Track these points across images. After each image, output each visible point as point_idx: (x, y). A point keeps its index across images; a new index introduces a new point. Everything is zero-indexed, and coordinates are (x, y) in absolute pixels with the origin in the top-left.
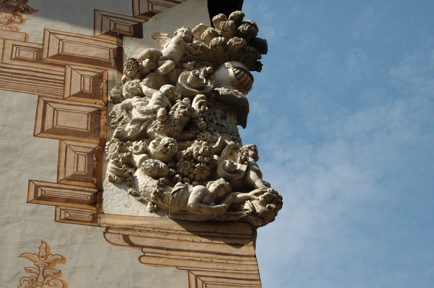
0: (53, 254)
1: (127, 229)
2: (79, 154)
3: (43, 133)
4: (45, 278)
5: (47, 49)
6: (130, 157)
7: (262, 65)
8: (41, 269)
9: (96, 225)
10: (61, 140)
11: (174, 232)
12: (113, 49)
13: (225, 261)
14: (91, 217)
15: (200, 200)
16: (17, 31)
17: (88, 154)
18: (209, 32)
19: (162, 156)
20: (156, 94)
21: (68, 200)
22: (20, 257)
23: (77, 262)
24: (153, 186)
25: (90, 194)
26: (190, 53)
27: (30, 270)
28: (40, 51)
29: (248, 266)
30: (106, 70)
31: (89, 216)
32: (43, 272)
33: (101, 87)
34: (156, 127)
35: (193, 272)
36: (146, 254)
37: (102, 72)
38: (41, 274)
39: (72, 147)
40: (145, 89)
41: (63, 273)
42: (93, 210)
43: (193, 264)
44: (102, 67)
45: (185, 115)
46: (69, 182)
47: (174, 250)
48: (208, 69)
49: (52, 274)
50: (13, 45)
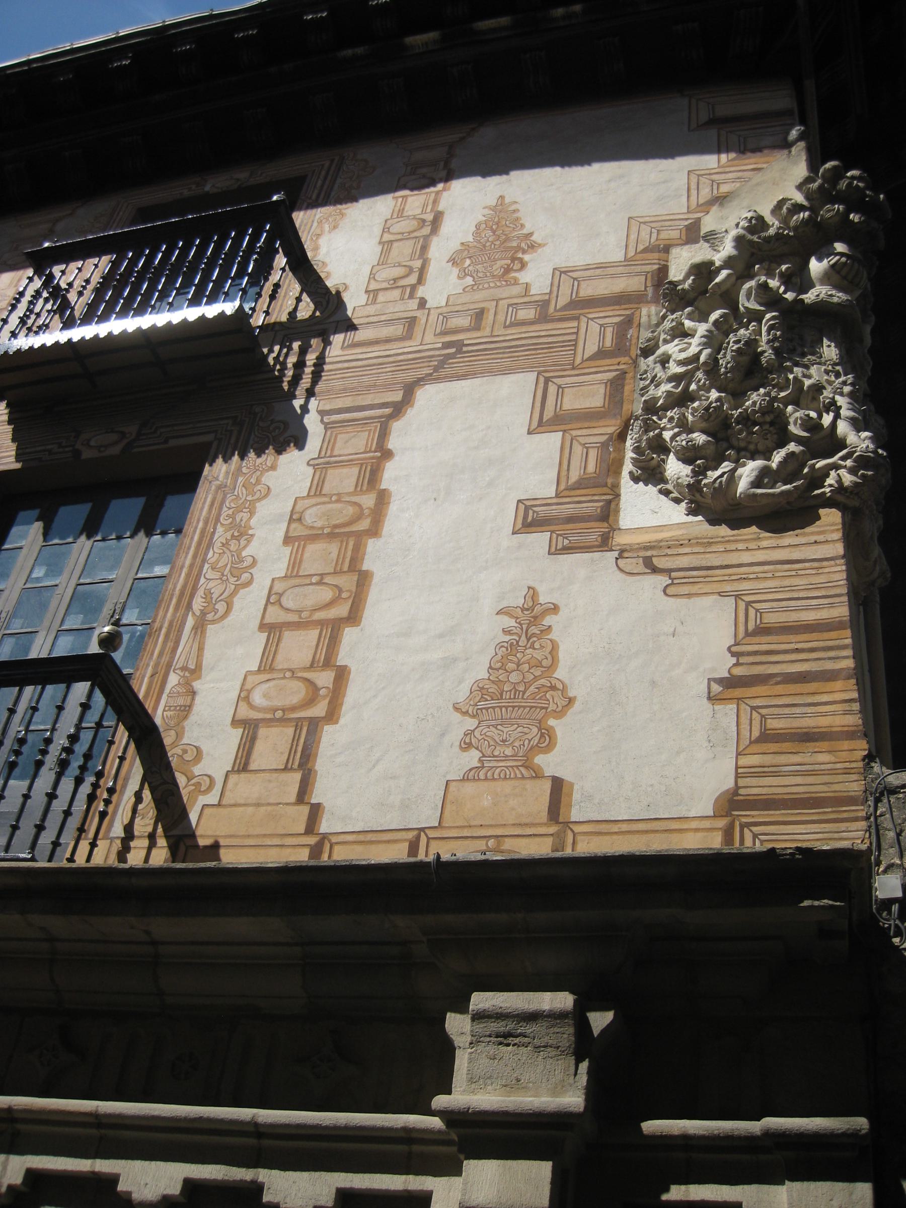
0: (543, 603)
1: (651, 548)
2: (589, 447)
3: (542, 426)
4: (528, 640)
5: (555, 299)
6: (660, 435)
7: (203, 315)
8: (524, 627)
9: (606, 549)
10: (564, 431)
11: (719, 539)
12: (652, 272)
13: (794, 573)
14: (599, 539)
15: (757, 483)
16: (516, 282)
17: (603, 444)
18: (787, 208)
19: (703, 425)
20: (702, 329)
21: (571, 519)
22: (497, 614)
23: (574, 610)
24: (687, 476)
25: (601, 504)
26: (760, 250)
27: (509, 631)
28: (545, 304)
29: (832, 575)
30: (637, 308)
31: (596, 538)
32: (527, 631)
33: (629, 336)
34: (699, 381)
35: (743, 597)
36: (675, 581)
37: (633, 314)
38: (524, 636)
39: (580, 439)
40: (688, 324)
41: (554, 628)
42: (603, 527)
43: (745, 585)
44: (631, 306)
45: (741, 353)
46: (573, 493)
47: (717, 568)
48: (784, 267)
49: (539, 632)
50: (509, 306)
